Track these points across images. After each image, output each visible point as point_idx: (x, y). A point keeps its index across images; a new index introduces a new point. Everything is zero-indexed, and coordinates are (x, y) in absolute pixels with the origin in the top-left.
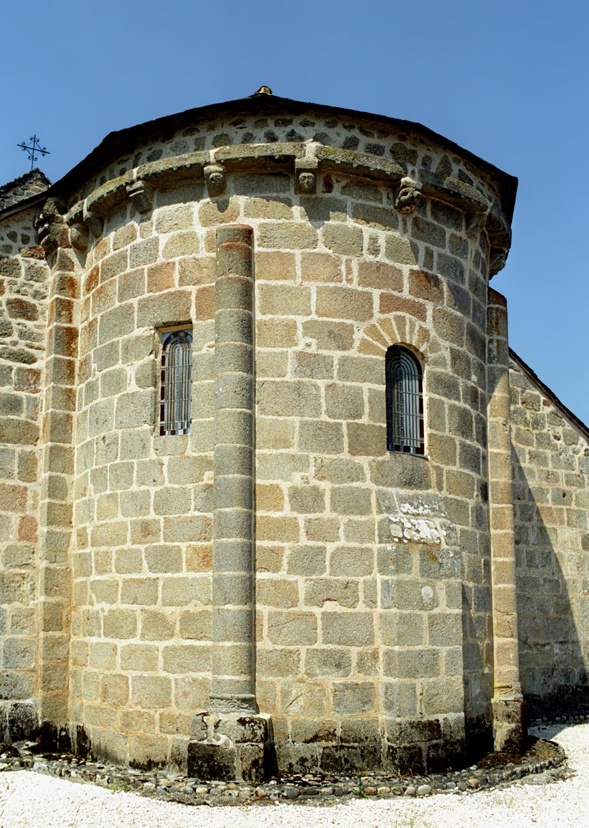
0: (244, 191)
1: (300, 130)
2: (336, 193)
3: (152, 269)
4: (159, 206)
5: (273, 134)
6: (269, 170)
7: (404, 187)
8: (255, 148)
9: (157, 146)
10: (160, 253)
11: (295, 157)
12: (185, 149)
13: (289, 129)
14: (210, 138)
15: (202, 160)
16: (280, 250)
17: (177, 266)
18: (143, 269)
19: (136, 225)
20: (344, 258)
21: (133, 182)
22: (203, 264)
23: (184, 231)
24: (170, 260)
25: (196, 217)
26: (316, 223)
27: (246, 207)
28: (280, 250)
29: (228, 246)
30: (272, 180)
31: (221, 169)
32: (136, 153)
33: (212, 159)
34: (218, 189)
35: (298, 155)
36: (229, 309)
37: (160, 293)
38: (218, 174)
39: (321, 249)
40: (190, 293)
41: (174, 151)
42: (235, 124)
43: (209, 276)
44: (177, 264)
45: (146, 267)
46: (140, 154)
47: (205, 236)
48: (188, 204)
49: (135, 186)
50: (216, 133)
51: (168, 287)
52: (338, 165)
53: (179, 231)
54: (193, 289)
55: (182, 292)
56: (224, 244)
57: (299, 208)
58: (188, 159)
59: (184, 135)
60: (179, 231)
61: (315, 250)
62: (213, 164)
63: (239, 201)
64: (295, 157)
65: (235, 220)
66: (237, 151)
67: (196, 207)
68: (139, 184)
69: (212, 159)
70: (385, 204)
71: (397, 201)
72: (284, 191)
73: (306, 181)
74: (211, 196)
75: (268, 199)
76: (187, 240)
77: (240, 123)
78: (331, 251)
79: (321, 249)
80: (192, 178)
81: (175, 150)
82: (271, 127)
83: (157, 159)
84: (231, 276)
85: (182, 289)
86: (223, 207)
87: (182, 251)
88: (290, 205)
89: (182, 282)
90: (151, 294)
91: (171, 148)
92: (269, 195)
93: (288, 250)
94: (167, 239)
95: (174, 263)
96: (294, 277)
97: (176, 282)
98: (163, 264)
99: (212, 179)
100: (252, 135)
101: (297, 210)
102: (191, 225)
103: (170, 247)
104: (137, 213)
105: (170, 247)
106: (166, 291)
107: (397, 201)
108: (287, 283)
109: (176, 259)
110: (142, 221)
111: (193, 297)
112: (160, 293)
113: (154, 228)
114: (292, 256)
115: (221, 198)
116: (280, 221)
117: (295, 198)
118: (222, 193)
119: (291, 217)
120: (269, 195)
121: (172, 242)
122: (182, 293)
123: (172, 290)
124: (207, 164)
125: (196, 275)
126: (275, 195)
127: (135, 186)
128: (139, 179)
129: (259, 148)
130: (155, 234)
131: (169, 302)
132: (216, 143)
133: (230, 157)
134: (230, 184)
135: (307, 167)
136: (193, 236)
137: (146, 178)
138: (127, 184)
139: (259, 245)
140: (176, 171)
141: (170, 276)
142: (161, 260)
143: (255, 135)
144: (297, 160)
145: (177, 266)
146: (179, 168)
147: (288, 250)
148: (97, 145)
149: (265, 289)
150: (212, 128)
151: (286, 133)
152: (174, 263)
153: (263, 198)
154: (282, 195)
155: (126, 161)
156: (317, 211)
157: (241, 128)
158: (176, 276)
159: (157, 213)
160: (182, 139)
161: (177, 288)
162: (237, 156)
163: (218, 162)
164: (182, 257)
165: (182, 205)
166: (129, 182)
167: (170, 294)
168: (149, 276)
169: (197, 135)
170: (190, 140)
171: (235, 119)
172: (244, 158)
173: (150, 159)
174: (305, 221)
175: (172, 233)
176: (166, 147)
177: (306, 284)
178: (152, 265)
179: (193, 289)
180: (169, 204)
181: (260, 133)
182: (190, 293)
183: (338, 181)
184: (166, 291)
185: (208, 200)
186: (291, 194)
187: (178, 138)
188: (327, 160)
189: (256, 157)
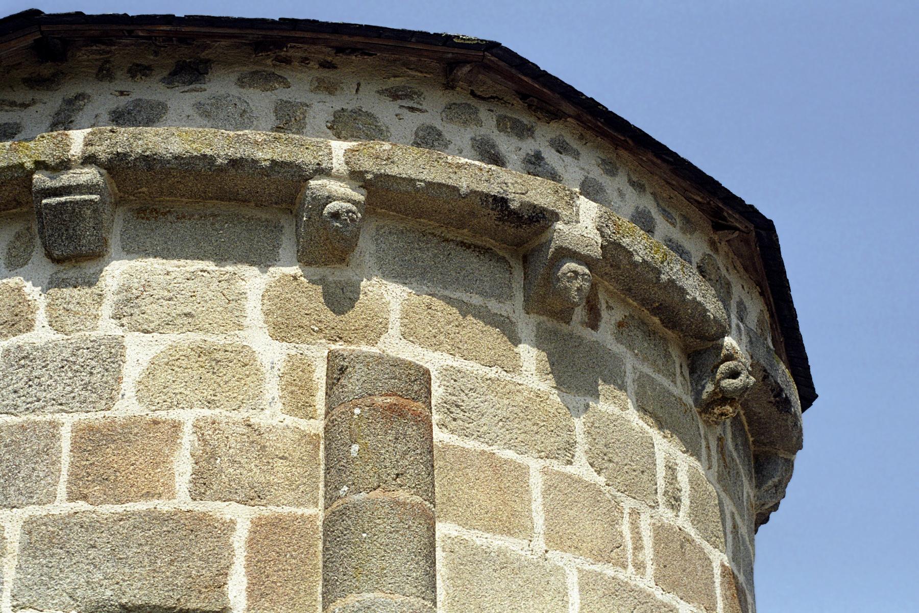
0: (400, 274)
1: (551, 157)
2: (605, 335)
3: (91, 429)
4: (133, 250)
5: (493, 146)
6: (465, 234)
7: (729, 358)
8: (459, 166)
9: (149, 91)
10: (128, 386)
11: (556, 217)
12: (244, 119)
13: (529, 146)
14: (321, 109)
15: (306, 158)
16: (495, 449)
17: (187, 438)
18: (54, 425)
19: (31, 291)
20: (628, 504)
21: (64, 165)
22: (270, 440)
23: (216, 339)
24: (162, 415)
25: (254, 309)
26: (571, 398)
27: (405, 315)
28: (495, 449)
29: (391, 408)
30: (473, 262)
31: (359, 197)
32: (70, 90)
33: (338, 163)
34: (328, 248)
35: (564, 213)
36: (399, 598)
37: (119, 508)
38: (349, 206)
39: (581, 468)
40: (230, 526)
41: (206, 115)
42: (394, 95)
43: (292, 485)
44: (188, 429)
45: (68, 422)
46: (80, 96)
47: (281, 366)
48: (230, 268)
49: (66, 179)
50: (337, 102)
51: (148, 495)
52: (635, 265)
53: (196, 337)
54: (241, 517)
55: (202, 519)
56: (379, 400)
57: (534, 352)
58: (262, 145)
59: (241, 83)
60: (196, 337)
61: (569, 469)
62: (339, 178)
63: (387, 296)
64: (556, 217)
65: (374, 343)
66: (410, 164)
67: (254, 282)
68: (89, 175)
69: (338, 163)
70: (679, 389)
71: (710, 388)
72: (499, 298)
73: (577, 283)
74: (305, 258)
75: (465, 309)
76: (221, 367)
77: (408, 96)
78: (601, 480)
79: (581, 468)
80: (245, 201)
81: (208, 113)
82: (488, 126)
83: (149, 122)
84: (402, 495)
85: (200, 507)
86: (341, 299)
87: (208, 394)
88: (516, 341)
89: (202, 484)
90: (82, 505)
91: (199, 106)
92: (465, 297)
93: (510, 454)
94: (155, 350)
95: (176, 426)
96: (526, 531)
97: (182, 482)
98: (133, 421)
99: (336, 215)
100: (440, 134)
101: (529, 356)
102: (240, 327)
103: (163, 376)
104: (38, 255)
105: (163, 376)
106: (141, 506)
107: (710, 388)
108: (513, 545)
109: (187, 417)
110: (56, 283)
111: (239, 539)
112: (119, 508)
113: (106, 310)
114: (522, 472)
115: (336, 274)
116: (492, 373)
117: (526, 324)
118: (342, 260)
119: (515, 369)
120: (465, 297)
121: (171, 361)
122: (199, 525)
123: (164, 506)
124: (323, 172)
125: (253, 473)
126: (476, 300)
127: (66, 179)
128: (89, 160)
129: (461, 170)
130: (107, 327)
131: (150, 541)
132: (340, 126)
133: (393, 170)
134: (366, 244)
135: (584, 251)
136: (245, 360)
137: (116, 166)
138: (40, 165)
139: (443, 425)
140: (221, 169)
141: (159, 461)
142: (128, 406)
143: (447, 136)
144: (559, 225)
145: (187, 438)
146: (235, 163)
147: (510, 454)
148: (87, 12)
149: (454, 545)
150: (330, 89)
151: (523, 154)
152: (176, 426)
153: (449, 301)
154: (493, 305)
155: (24, 106)
156: (577, 372)
157: (412, 109)
158: (183, 467)
159: (117, 272)
160: (235, 91)
161: (181, 499)
162: (412, 173)
163: (356, 176)
164: (207, 412)
165: (210, 265)
166: (50, 160)
167: (154, 517)
168: (76, 447)
169: (282, 94)
170: (261, 100)
171: (393, 82)
172: (430, 184)
173: (119, 118)
174: (545, 385)
175: (171, 337)
176: (180, 100)
177: (555, 556)
178: (95, 417)
179: (241, 517)
180: (166, 254)
181: (461, 135)
182: (230, 526)
183: (609, 308)
184: (141, 506)
185: (295, 270)
186: (514, 308)
187: (221, 85)
188: (561, 247)
189: (463, 190)
